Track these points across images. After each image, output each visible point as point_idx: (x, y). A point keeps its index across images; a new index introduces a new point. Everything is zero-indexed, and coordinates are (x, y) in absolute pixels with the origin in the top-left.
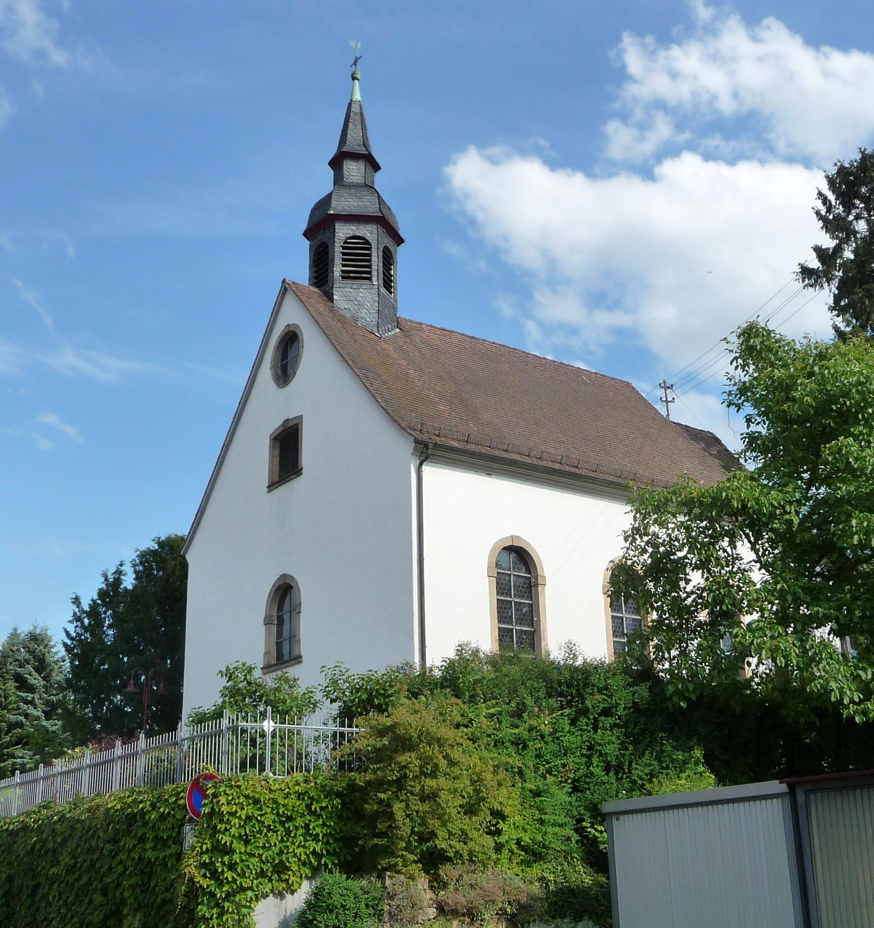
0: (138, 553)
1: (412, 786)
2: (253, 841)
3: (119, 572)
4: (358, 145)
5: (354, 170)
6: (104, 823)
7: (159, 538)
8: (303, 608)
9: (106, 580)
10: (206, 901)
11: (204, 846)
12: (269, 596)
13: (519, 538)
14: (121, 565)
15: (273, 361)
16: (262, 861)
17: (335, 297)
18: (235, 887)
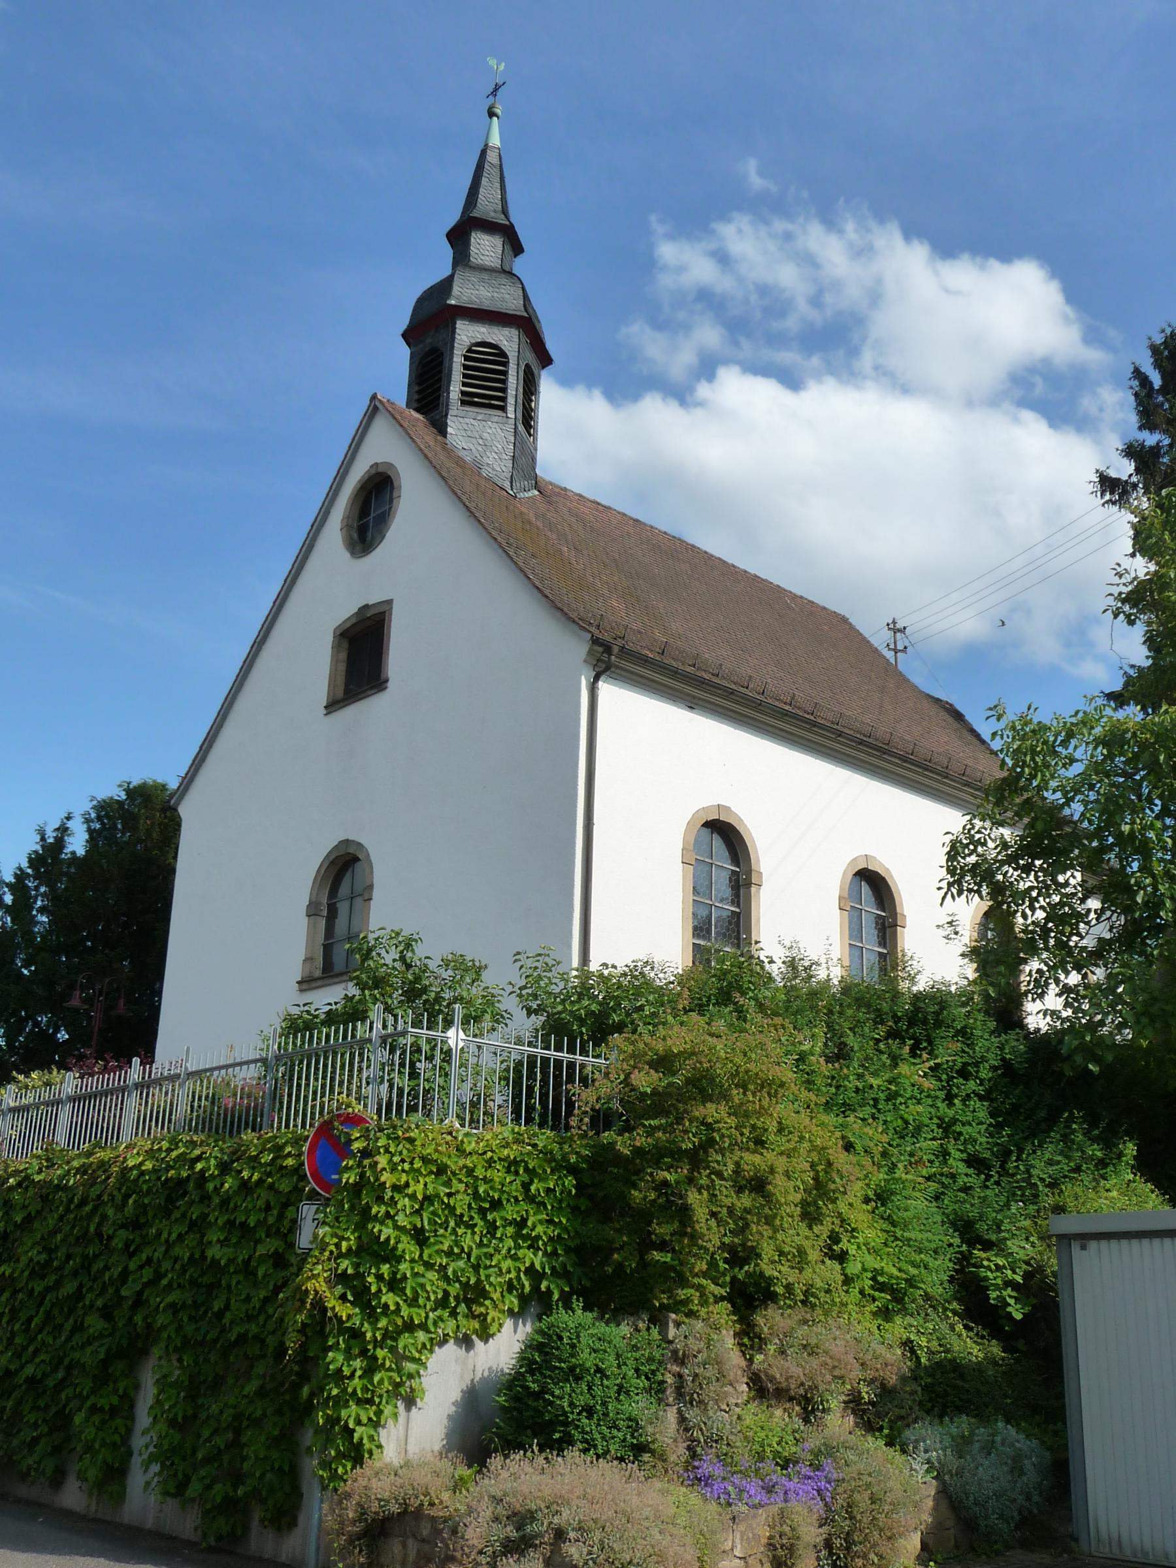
0: (95, 803)
1: (718, 1162)
2: (432, 1240)
3: (63, 830)
4: (495, 211)
5: (486, 248)
6: (115, 1193)
7: (129, 783)
8: (376, 894)
9: (43, 839)
10: (342, 1345)
11: (344, 1244)
12: (318, 871)
13: (728, 809)
14: (68, 818)
15: (347, 517)
16: (446, 1278)
17: (449, 430)
18: (399, 1322)
